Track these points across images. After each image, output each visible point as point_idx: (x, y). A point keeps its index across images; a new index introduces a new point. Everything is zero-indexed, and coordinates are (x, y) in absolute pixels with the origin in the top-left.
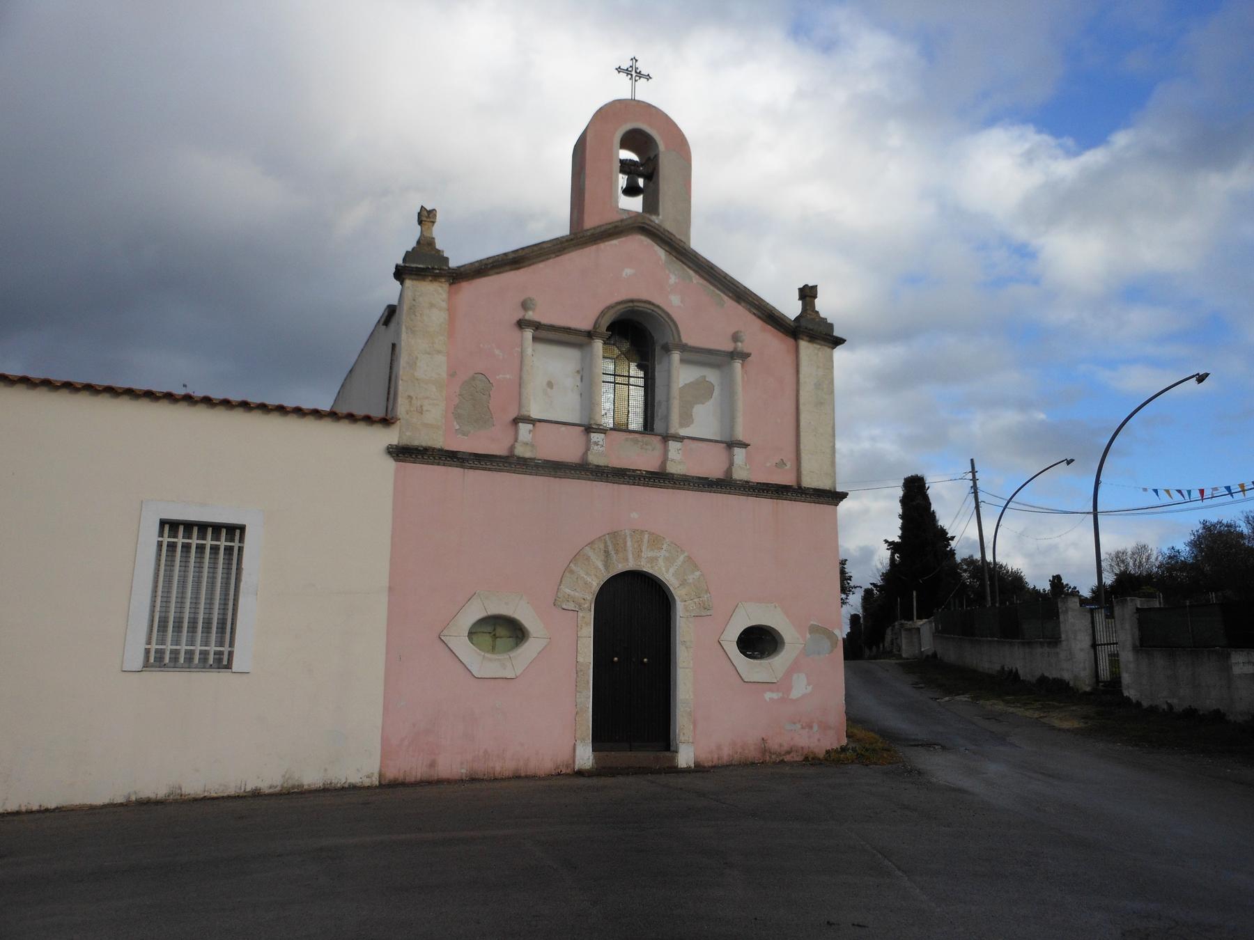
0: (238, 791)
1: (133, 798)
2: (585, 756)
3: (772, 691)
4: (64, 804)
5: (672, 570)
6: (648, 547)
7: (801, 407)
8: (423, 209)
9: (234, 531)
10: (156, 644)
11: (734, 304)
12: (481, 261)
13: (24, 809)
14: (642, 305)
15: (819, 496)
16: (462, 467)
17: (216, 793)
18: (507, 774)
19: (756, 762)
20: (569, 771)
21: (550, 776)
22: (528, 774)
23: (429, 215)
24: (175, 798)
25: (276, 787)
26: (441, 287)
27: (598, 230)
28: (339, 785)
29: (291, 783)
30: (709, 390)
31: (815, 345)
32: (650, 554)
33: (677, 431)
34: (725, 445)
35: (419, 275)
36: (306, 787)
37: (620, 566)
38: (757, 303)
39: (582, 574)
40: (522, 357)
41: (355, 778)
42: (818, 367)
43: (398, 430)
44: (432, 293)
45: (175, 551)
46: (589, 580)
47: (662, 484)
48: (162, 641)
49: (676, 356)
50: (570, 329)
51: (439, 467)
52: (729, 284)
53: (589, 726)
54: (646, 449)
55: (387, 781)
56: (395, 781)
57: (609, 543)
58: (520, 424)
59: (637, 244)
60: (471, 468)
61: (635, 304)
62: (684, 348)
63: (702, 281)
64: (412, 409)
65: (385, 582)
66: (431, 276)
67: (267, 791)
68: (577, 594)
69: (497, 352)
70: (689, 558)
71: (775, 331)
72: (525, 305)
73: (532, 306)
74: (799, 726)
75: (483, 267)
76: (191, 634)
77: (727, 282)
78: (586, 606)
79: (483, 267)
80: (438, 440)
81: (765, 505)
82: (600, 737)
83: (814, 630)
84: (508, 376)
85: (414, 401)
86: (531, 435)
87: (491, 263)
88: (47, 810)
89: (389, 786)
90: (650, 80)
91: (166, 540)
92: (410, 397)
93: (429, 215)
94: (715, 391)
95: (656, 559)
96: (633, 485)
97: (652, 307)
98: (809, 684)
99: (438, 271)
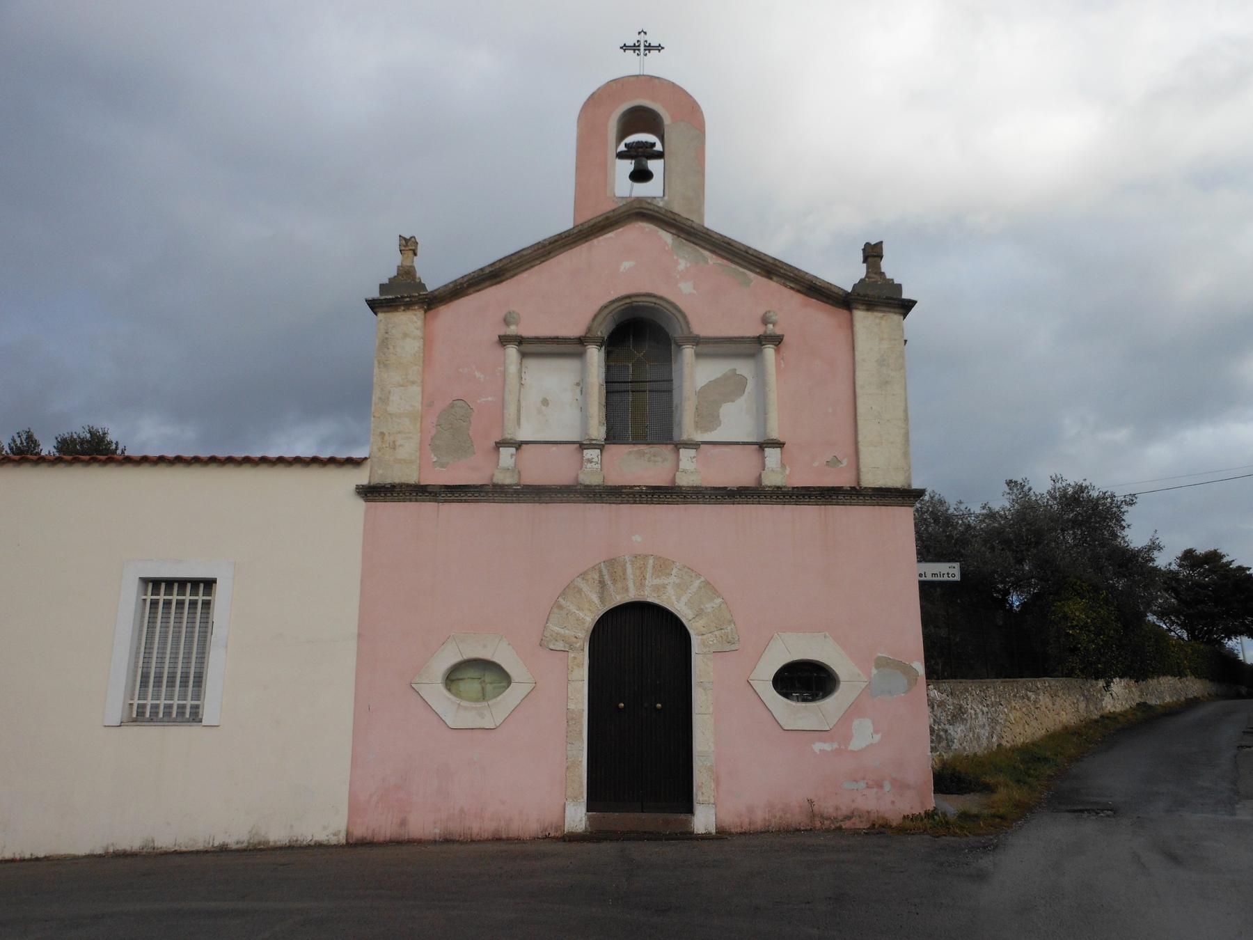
0: (206, 846)
1: (111, 850)
2: (577, 817)
3: (824, 741)
4: (52, 853)
5: (684, 599)
6: (653, 574)
7: (859, 390)
8: (413, 239)
9: (209, 584)
10: (178, 700)
11: (764, 280)
12: (455, 281)
13: (18, 857)
14: (644, 299)
15: (884, 496)
16: (436, 501)
17: (186, 847)
18: (486, 835)
19: (802, 828)
20: (558, 834)
21: (535, 839)
22: (510, 836)
23: (407, 243)
24: (149, 850)
25: (242, 843)
26: (415, 315)
27: (586, 226)
28: (305, 843)
29: (255, 840)
30: (741, 384)
31: (876, 314)
32: (658, 581)
33: (692, 437)
34: (757, 446)
35: (391, 306)
36: (272, 844)
37: (653, 599)
38: (792, 275)
39: (573, 609)
40: (504, 376)
41: (321, 836)
42: (881, 339)
43: (369, 469)
44: (408, 322)
45: (171, 608)
46: (581, 615)
47: (670, 500)
48: (143, 696)
49: (688, 351)
50: (557, 338)
51: (412, 503)
52: (752, 258)
53: (582, 783)
54: (655, 462)
55: (354, 840)
56: (363, 840)
57: (605, 572)
58: (766, 449)
59: (638, 233)
60: (445, 501)
61: (634, 299)
62: (697, 341)
63: (720, 261)
64: (384, 446)
65: (354, 630)
66: (404, 305)
67: (235, 847)
68: (567, 631)
69: (477, 374)
70: (707, 583)
71: (822, 303)
72: (506, 322)
73: (512, 320)
74: (862, 784)
75: (459, 287)
76: (157, 689)
77: (749, 256)
78: (578, 644)
79: (459, 287)
80: (410, 476)
81: (810, 514)
82: (597, 797)
83: (881, 663)
84: (490, 399)
85: (386, 437)
86: (513, 459)
87: (466, 282)
88: (37, 859)
89: (355, 845)
90: (662, 51)
91: (149, 597)
92: (382, 434)
93: (407, 243)
94: (748, 385)
95: (664, 586)
96: (634, 503)
97: (653, 300)
98: (876, 731)
99: (408, 299)
